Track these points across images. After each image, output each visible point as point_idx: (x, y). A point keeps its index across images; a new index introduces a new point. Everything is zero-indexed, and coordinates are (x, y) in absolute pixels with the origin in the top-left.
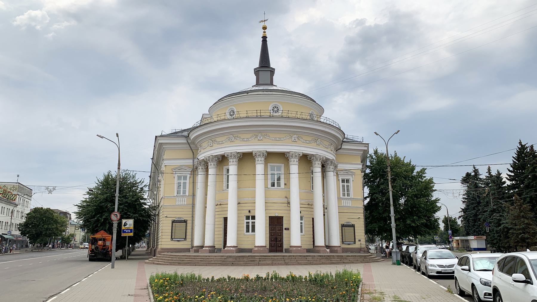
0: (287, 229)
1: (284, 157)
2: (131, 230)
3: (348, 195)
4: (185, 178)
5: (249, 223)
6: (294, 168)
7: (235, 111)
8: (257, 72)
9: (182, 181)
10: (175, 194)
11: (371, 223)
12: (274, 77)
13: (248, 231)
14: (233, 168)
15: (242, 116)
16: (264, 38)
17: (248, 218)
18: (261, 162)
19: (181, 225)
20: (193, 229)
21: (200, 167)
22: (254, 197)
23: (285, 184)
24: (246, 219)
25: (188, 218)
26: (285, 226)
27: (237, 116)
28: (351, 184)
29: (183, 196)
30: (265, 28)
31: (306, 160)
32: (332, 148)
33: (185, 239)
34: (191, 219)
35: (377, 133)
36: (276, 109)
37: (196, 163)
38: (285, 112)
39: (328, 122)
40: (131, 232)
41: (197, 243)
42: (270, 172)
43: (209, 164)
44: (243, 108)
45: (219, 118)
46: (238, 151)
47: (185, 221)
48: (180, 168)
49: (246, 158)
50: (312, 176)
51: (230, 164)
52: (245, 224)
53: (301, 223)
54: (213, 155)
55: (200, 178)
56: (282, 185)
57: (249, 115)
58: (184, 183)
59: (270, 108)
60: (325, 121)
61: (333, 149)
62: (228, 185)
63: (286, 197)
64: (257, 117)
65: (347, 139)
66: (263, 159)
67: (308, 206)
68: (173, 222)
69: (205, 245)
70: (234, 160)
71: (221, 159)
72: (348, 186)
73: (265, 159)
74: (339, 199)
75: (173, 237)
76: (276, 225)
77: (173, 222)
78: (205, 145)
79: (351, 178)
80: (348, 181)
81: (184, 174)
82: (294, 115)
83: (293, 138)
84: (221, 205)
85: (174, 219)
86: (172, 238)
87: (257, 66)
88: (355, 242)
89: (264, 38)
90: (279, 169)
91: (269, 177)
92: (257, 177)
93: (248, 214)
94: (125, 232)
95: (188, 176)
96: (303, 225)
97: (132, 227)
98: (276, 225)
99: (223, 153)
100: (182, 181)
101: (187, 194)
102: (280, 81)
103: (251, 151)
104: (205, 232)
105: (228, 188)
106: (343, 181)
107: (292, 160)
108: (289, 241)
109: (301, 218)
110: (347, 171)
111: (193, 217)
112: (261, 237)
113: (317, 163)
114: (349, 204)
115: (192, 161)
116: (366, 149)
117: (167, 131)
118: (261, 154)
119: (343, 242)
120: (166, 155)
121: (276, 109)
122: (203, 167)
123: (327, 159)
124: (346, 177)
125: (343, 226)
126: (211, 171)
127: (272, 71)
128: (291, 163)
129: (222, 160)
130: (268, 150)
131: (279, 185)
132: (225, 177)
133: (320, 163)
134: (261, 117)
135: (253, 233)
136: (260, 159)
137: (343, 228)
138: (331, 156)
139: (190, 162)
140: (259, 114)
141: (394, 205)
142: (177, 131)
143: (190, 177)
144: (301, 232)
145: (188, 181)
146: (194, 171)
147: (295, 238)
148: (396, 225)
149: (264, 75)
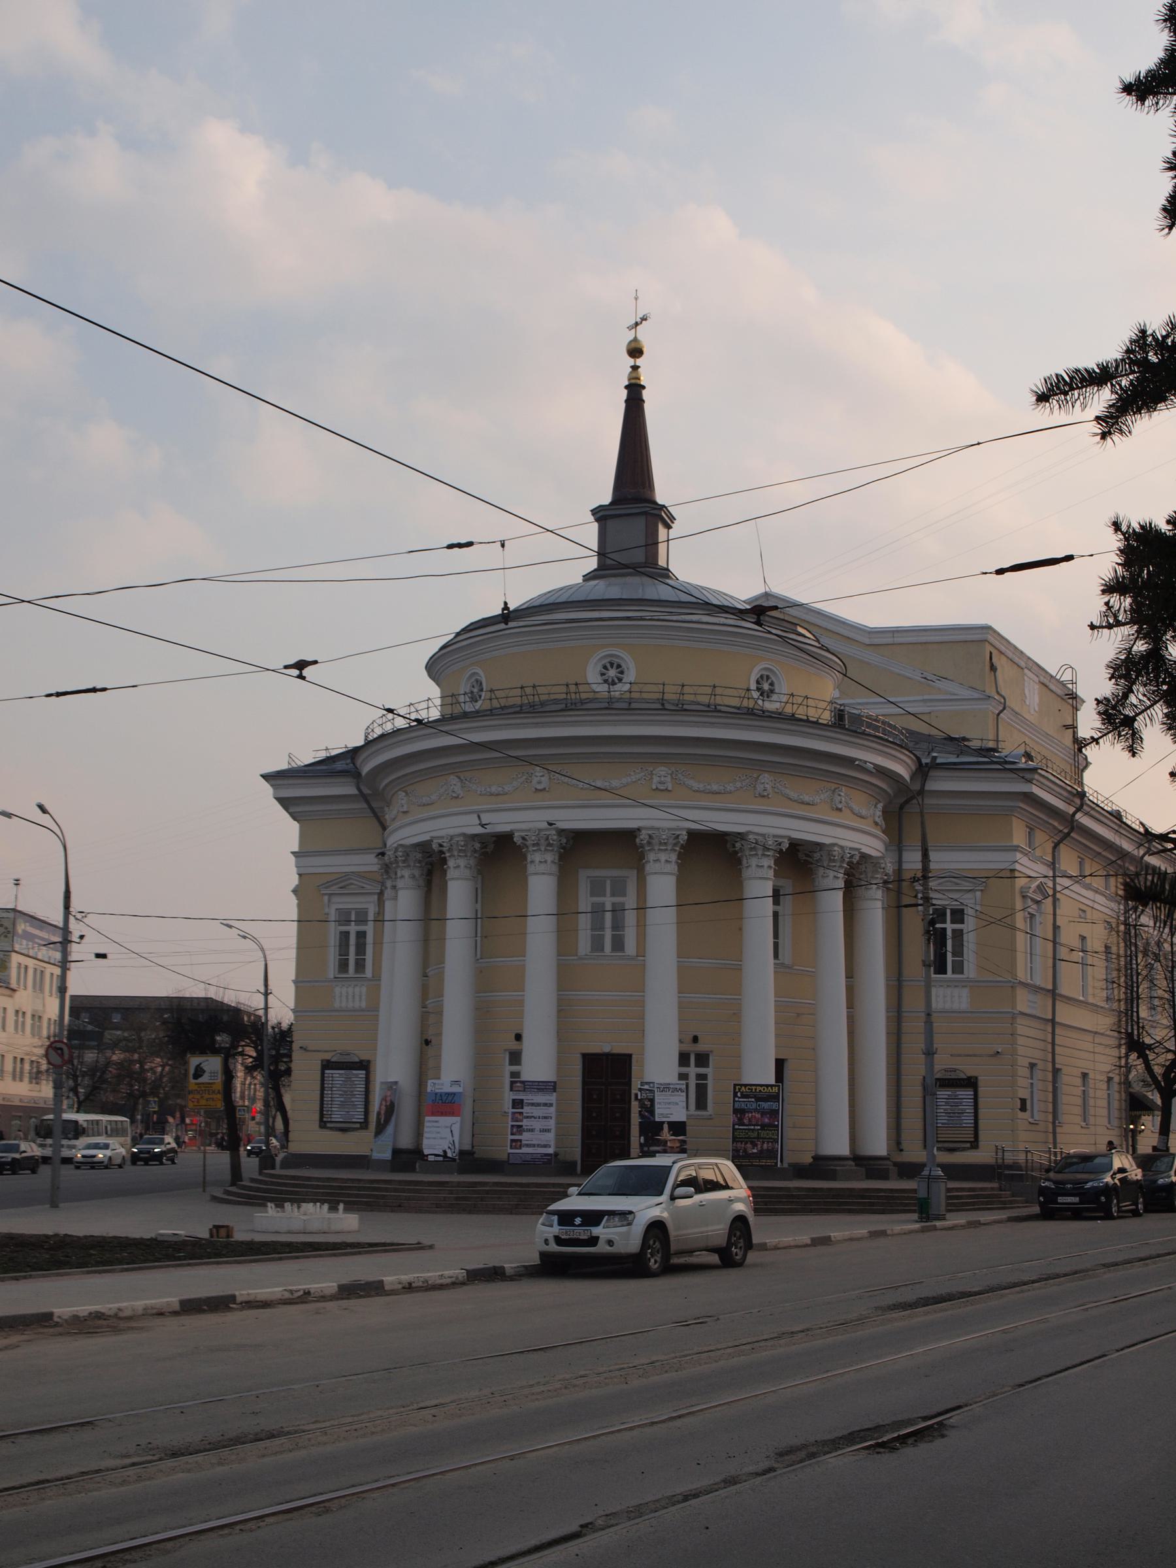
1: (625, 845)
6: (662, 885)
9: (353, 929)
10: (332, 970)
16: (635, 391)
24: (511, 1064)
42: (585, 902)
49: (498, 853)
68: (327, 1065)
77: (327, 1065)
78: (401, 800)
83: (656, 779)
85: (327, 1056)
87: (606, 498)
88: (975, 1144)
89: (635, 391)
91: (584, 921)
92: (533, 924)
96: (710, 1083)
99: (426, 837)
117: (306, 758)
121: (613, 668)
136: (537, 857)
142: (334, 753)
149: (631, 531)
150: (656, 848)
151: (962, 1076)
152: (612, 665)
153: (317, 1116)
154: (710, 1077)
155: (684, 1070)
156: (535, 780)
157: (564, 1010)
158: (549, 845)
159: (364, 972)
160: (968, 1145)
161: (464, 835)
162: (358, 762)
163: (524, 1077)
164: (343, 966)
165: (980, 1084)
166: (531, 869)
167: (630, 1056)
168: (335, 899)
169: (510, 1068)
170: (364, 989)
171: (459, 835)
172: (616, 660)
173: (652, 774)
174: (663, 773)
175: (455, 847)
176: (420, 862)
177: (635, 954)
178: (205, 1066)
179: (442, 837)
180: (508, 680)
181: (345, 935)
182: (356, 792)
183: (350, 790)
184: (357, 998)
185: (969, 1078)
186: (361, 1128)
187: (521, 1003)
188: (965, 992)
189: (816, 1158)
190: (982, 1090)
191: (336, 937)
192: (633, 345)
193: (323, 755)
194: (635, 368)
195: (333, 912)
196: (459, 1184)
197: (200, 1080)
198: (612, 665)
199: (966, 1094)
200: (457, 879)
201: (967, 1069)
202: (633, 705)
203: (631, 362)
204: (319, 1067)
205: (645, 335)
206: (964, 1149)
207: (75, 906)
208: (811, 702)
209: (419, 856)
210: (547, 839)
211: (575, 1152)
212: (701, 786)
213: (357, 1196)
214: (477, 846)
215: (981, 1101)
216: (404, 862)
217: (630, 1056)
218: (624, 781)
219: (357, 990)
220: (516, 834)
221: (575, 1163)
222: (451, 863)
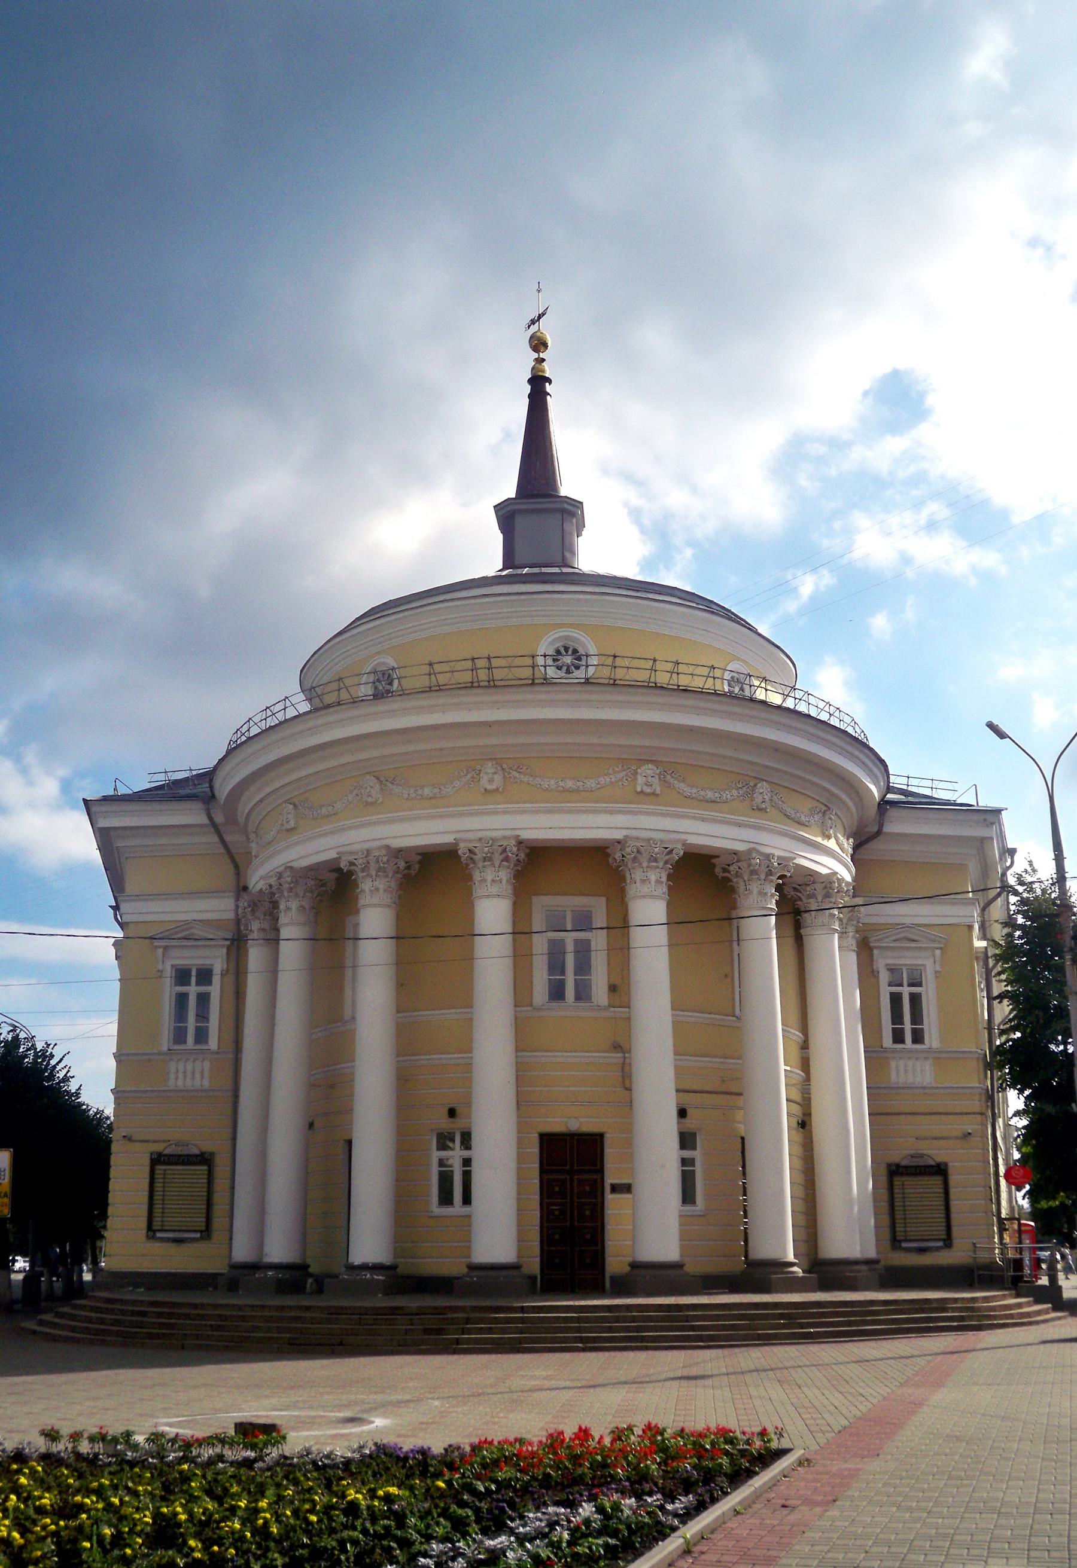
0: (627, 1188)
1: (600, 865)
3: (918, 1037)
4: (205, 976)
6: (650, 907)
8: (507, 515)
10: (165, 1042)
13: (446, 1198)
14: (374, 918)
16: (538, 384)
18: (495, 890)
19: (193, 1172)
23: (613, 989)
26: (611, 1177)
41: (242, 1253)
47: (205, 1159)
49: (432, 876)
55: (255, 956)
56: (600, 993)
57: (442, 679)
59: (545, 646)
63: (617, 1047)
64: (472, 686)
66: (505, 875)
68: (157, 1160)
69: (268, 1260)
70: (381, 884)
71: (332, 886)
75: (156, 1225)
76: (573, 1172)
77: (157, 1160)
82: (644, 676)
83: (641, 780)
85: (159, 1148)
86: (151, 1230)
87: (509, 490)
88: (948, 1241)
89: (538, 384)
90: (583, 922)
93: (445, 1124)
98: (573, 1172)
100: (193, 990)
102: (598, 550)
103: (448, 839)
109: (686, 1140)
112: (499, 1225)
118: (494, 851)
119: (896, 1243)
128: (632, 890)
130: (526, 835)
131: (583, 993)
134: (492, 685)
135: (466, 1210)
136: (489, 875)
137: (898, 1181)
139: (220, 908)
140: (483, 675)
141: (755, 1492)
147: (650, 1222)
152: (566, 649)
153: (143, 1222)
154: (698, 1163)
155: (687, 1154)
156: (484, 781)
157: (523, 1075)
158: (507, 859)
160: (941, 1244)
161: (388, 847)
162: (217, 783)
164: (179, 1036)
165: (951, 1171)
166: (478, 891)
167: (601, 1136)
169: (436, 1155)
170: (207, 1065)
171: (379, 848)
173: (636, 773)
174: (650, 772)
175: (372, 864)
176: (311, 892)
177: (606, 1004)
181: (181, 1000)
182: (206, 821)
184: (198, 1075)
185: (938, 1165)
186: (202, 1238)
187: (467, 1068)
188: (928, 1066)
189: (635, 1266)
190: (954, 1179)
191: (179, 995)
193: (160, 779)
195: (168, 968)
196: (421, 1312)
198: (566, 649)
199: (936, 1181)
200: (375, 905)
201: (937, 1153)
202: (618, 682)
203: (536, 355)
204: (147, 1162)
205: (547, 329)
206: (938, 1249)
208: (812, 700)
210: (504, 851)
211: (533, 1266)
212: (694, 791)
214: (402, 864)
215: (953, 1191)
217: (601, 1136)
219: (198, 1064)
220: (462, 845)
221: (536, 1278)
222: (366, 885)
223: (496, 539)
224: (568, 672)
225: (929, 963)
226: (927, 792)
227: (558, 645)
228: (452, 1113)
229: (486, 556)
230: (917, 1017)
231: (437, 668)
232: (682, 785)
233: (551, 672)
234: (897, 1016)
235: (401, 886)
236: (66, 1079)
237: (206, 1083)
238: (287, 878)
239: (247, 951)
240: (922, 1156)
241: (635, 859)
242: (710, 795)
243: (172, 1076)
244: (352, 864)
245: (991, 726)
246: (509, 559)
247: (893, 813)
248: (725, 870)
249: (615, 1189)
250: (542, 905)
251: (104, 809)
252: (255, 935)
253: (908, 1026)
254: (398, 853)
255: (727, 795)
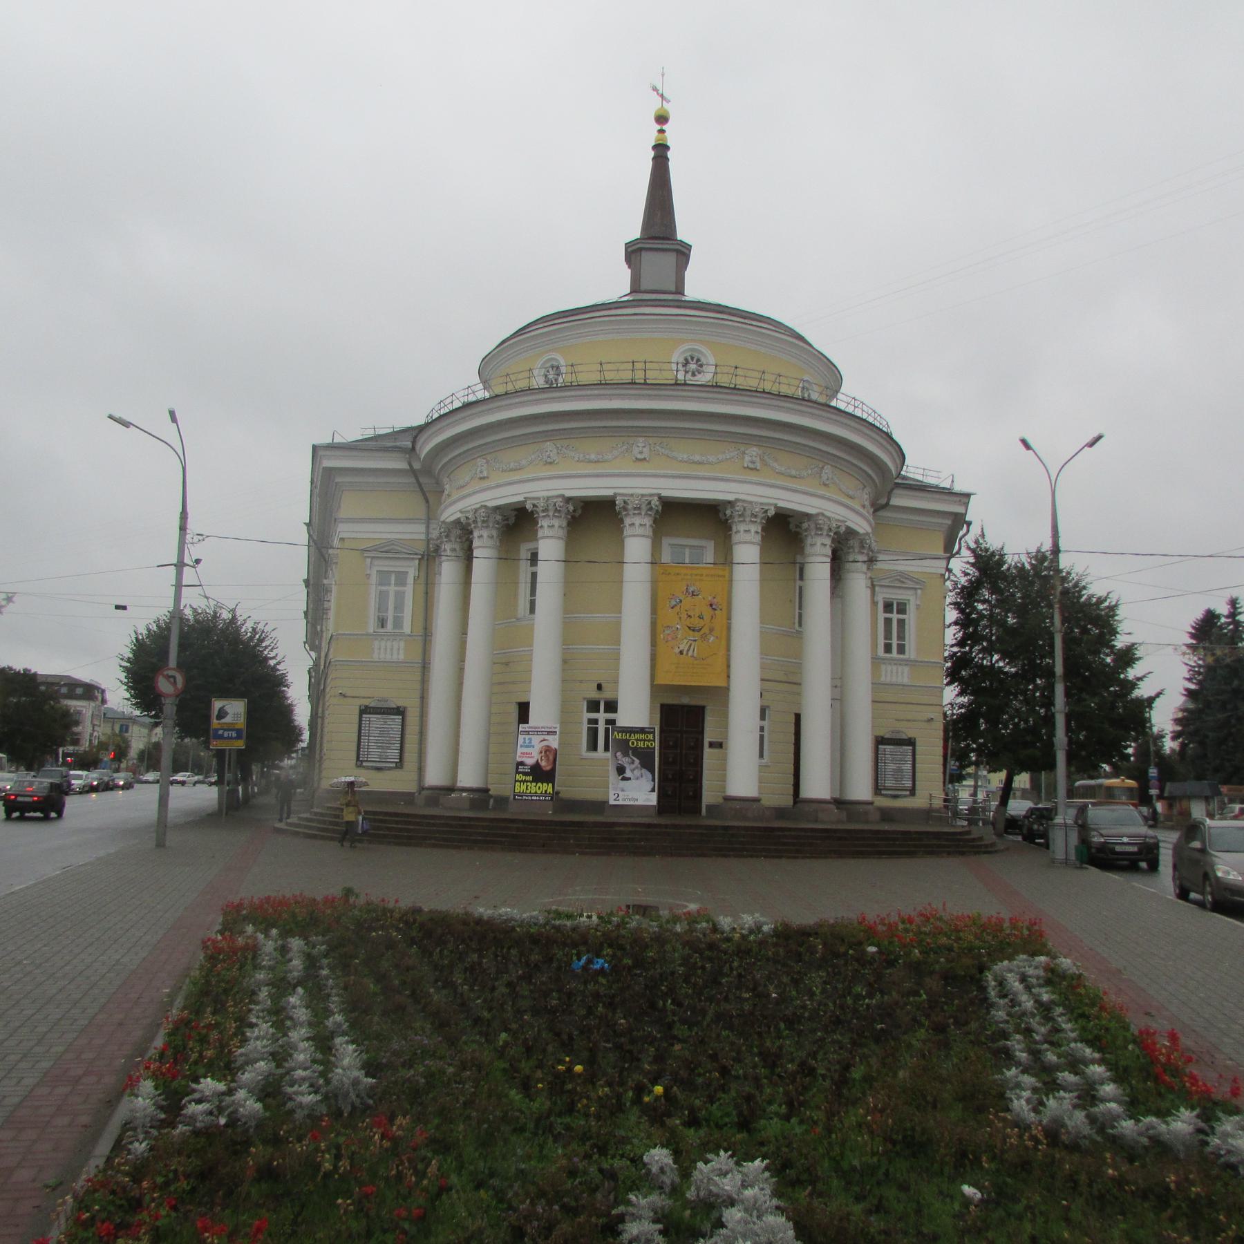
0: (719, 745)
1: (711, 517)
2: (239, 731)
3: (901, 649)
4: (401, 578)
5: (596, 721)
6: (748, 550)
7: (562, 362)
8: (633, 253)
10: (372, 627)
11: (957, 738)
12: (689, 274)
13: (593, 746)
14: (550, 543)
15: (584, 378)
16: (661, 151)
17: (593, 706)
18: (640, 531)
20: (422, 734)
21: (448, 547)
22: (617, 640)
24: (589, 711)
25: (410, 702)
27: (568, 379)
28: (911, 617)
29: (395, 635)
30: (662, 119)
31: (784, 530)
32: (865, 497)
33: (400, 764)
34: (417, 702)
35: (1030, 441)
36: (692, 361)
37: (434, 534)
38: (726, 370)
39: (858, 413)
40: (239, 737)
41: (435, 776)
43: (476, 534)
44: (588, 358)
45: (510, 387)
46: (569, 494)
47: (400, 711)
48: (386, 550)
49: (593, 517)
50: (799, 583)
51: (540, 534)
52: (585, 726)
53: (762, 729)
54: (490, 504)
55: (448, 570)
58: (397, 593)
59: (677, 357)
60: (850, 409)
61: (867, 503)
62: (533, 603)
65: (905, 478)
66: (648, 521)
67: (783, 680)
68: (365, 710)
69: (459, 784)
70: (556, 522)
71: (512, 521)
72: (901, 623)
73: (655, 521)
74: (876, 661)
76: (683, 729)
79: (912, 599)
80: (902, 609)
81: (399, 566)
83: (747, 458)
84: (508, 664)
85: (366, 702)
87: (636, 233)
88: (913, 791)
89: (661, 151)
93: (594, 694)
94: (221, 737)
95: (412, 573)
96: (766, 734)
97: (241, 722)
99: (520, 498)
100: (392, 589)
101: (407, 629)
103: (610, 493)
104: (457, 743)
105: (532, 610)
106: (888, 607)
107: (742, 527)
108: (723, 779)
110: (902, 579)
111: (423, 698)
113: (819, 541)
114: (902, 675)
115: (422, 528)
116: (960, 510)
117: (352, 434)
119: (878, 789)
120: (349, 506)
121: (692, 361)
122: (457, 547)
123: (851, 533)
124: (896, 596)
125: (880, 741)
126: (483, 566)
127: (683, 253)
128: (735, 538)
129: (517, 522)
130: (665, 493)
132: (524, 589)
133: (828, 541)
138: (861, 525)
139: (414, 532)
143: (416, 579)
144: (761, 756)
145: (409, 590)
146: (429, 558)
147: (739, 771)
148: (1070, 742)
149: (658, 265)
150: (748, 519)
151: (904, 737)
156: (636, 450)
159: (402, 628)
161: (563, 496)
163: (619, 724)
165: (918, 744)
168: (376, 562)
170: (402, 644)
171: (558, 496)
172: (696, 355)
178: (229, 709)
179: (538, 498)
180: (546, 383)
183: (402, 465)
184: (395, 652)
186: (396, 767)
190: (919, 749)
192: (661, 113)
193: (370, 433)
194: (662, 131)
197: (223, 721)
198: (692, 358)
201: (910, 734)
204: (357, 712)
206: (905, 796)
207: (193, 526)
208: (865, 408)
209: (499, 518)
210: (650, 503)
213: (401, 830)
214: (571, 508)
216: (483, 522)
218: (721, 457)
222: (544, 523)
223: (626, 273)
224: (694, 375)
225: (912, 599)
226: (920, 478)
227: (688, 354)
228: (599, 687)
229: (614, 282)
230: (901, 636)
231: (605, 367)
232: (775, 465)
233: (681, 376)
234: (888, 635)
235: (569, 524)
236: (1120, 622)
237: (402, 657)
238: (482, 512)
239: (440, 563)
240: (898, 732)
241: (741, 516)
242: (793, 472)
243: (376, 651)
244: (534, 506)
245: (1100, 437)
246: (634, 290)
247: (897, 491)
248: (797, 526)
249: (711, 745)
250: (666, 542)
251: (328, 453)
252: (448, 553)
253: (895, 642)
254: (569, 500)
255: (804, 473)
